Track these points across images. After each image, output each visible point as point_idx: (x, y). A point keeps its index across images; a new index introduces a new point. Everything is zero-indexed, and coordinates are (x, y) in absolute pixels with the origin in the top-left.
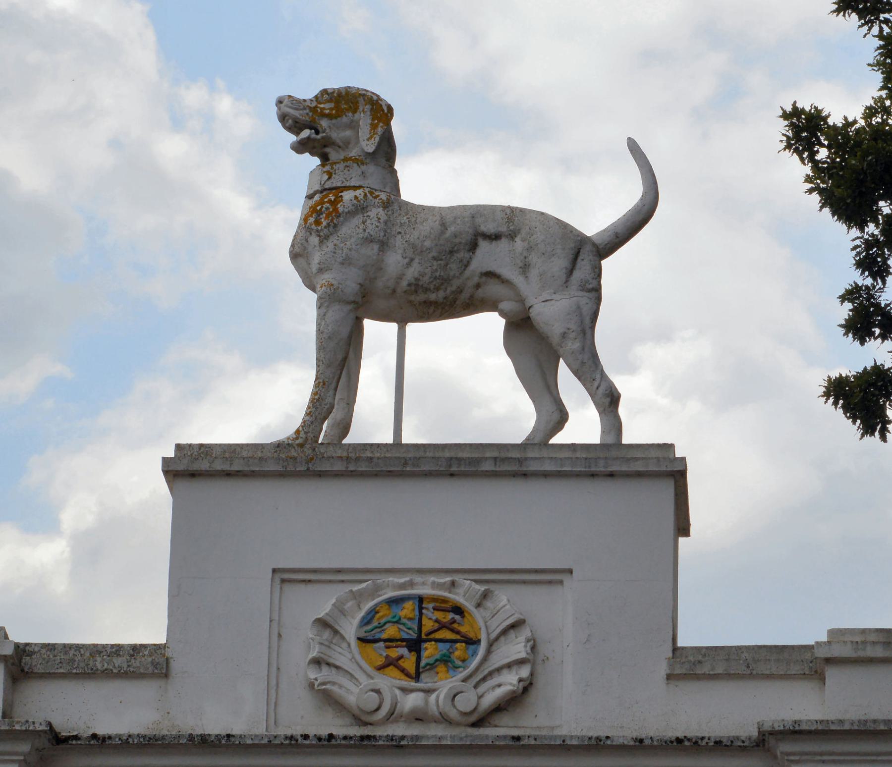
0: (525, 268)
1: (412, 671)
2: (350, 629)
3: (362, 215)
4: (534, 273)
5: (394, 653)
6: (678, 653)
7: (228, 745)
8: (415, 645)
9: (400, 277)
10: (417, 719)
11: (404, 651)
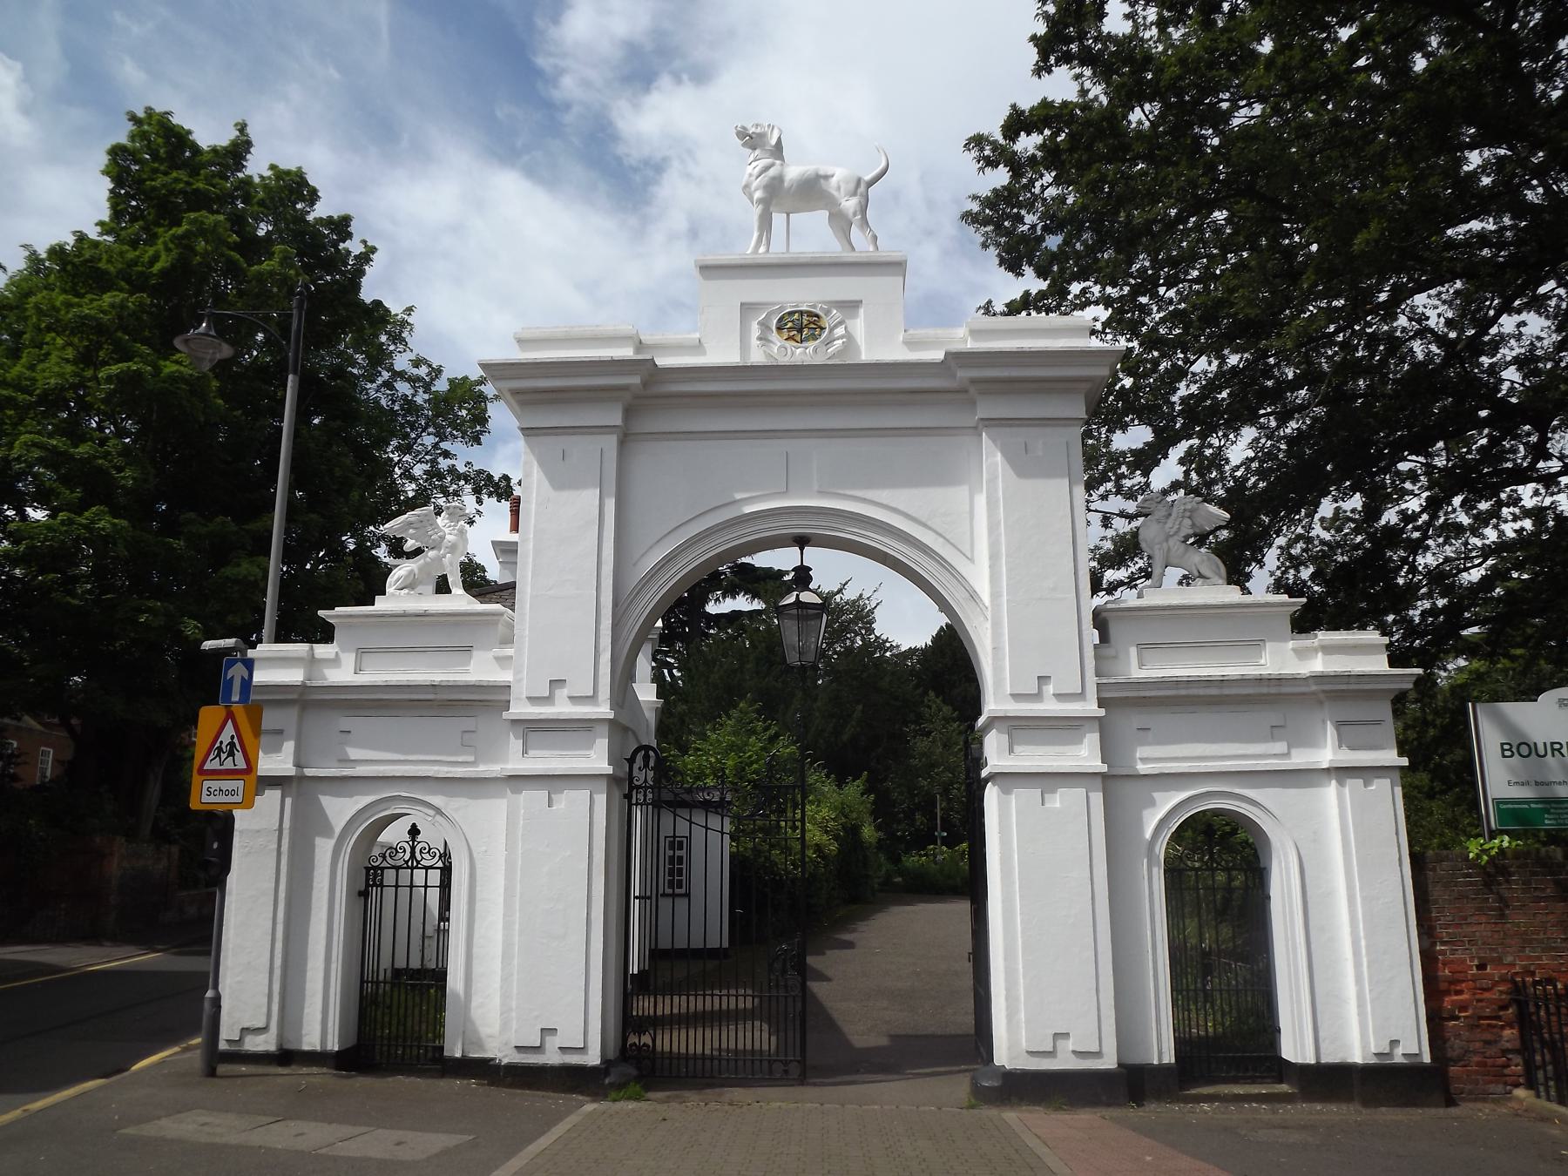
8: (800, 331)
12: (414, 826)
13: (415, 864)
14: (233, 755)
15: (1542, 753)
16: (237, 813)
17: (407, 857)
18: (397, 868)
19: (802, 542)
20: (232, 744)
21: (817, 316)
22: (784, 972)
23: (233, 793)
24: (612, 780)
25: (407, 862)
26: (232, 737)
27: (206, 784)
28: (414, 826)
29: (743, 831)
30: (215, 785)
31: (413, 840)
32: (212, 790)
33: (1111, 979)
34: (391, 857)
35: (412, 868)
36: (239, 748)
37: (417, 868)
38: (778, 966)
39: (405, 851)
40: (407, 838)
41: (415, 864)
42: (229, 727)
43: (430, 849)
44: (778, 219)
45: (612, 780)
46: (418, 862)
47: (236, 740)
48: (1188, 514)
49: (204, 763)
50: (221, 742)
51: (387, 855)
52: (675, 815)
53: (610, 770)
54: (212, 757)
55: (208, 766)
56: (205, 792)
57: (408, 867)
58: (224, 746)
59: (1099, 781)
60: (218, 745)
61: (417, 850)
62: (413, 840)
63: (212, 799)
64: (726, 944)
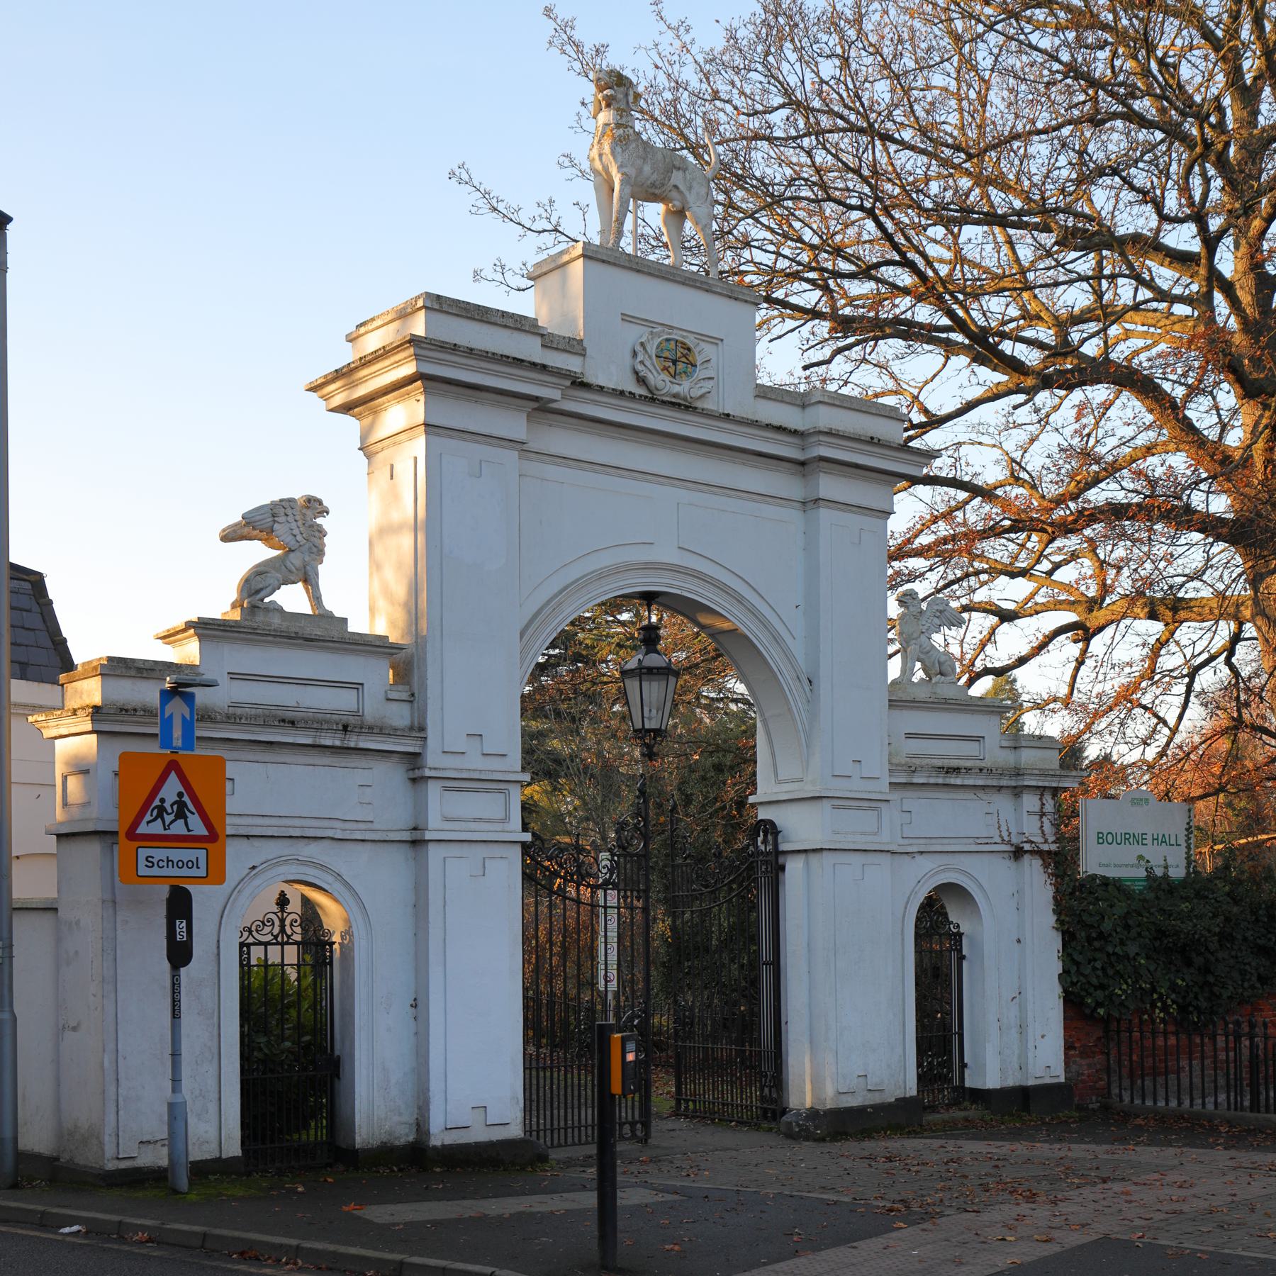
0: (690, 188)
1: (673, 374)
2: (652, 348)
3: (1090, 572)
4: (693, 191)
5: (667, 364)
6: (301, 575)
7: (958, 326)
8: (675, 362)
9: (648, 179)
10: (392, 477)
11: (671, 364)
13: (285, 939)
14: (185, 818)
18: (266, 944)
20: (181, 805)
21: (689, 349)
24: (220, 1157)
26: (180, 795)
27: (143, 853)
28: (283, 894)
30: (159, 854)
31: (282, 911)
32: (155, 861)
33: (431, 896)
34: (257, 931)
35: (282, 944)
36: (193, 810)
37: (288, 943)
39: (273, 924)
40: (275, 908)
41: (285, 939)
43: (263, 922)
45: (220, 1157)
46: (289, 937)
47: (186, 799)
50: (162, 800)
51: (253, 928)
53: (1000, 347)
54: (148, 817)
55: (143, 829)
56: (142, 862)
57: (277, 944)
58: (167, 805)
60: (157, 802)
61: (287, 922)
62: (282, 911)
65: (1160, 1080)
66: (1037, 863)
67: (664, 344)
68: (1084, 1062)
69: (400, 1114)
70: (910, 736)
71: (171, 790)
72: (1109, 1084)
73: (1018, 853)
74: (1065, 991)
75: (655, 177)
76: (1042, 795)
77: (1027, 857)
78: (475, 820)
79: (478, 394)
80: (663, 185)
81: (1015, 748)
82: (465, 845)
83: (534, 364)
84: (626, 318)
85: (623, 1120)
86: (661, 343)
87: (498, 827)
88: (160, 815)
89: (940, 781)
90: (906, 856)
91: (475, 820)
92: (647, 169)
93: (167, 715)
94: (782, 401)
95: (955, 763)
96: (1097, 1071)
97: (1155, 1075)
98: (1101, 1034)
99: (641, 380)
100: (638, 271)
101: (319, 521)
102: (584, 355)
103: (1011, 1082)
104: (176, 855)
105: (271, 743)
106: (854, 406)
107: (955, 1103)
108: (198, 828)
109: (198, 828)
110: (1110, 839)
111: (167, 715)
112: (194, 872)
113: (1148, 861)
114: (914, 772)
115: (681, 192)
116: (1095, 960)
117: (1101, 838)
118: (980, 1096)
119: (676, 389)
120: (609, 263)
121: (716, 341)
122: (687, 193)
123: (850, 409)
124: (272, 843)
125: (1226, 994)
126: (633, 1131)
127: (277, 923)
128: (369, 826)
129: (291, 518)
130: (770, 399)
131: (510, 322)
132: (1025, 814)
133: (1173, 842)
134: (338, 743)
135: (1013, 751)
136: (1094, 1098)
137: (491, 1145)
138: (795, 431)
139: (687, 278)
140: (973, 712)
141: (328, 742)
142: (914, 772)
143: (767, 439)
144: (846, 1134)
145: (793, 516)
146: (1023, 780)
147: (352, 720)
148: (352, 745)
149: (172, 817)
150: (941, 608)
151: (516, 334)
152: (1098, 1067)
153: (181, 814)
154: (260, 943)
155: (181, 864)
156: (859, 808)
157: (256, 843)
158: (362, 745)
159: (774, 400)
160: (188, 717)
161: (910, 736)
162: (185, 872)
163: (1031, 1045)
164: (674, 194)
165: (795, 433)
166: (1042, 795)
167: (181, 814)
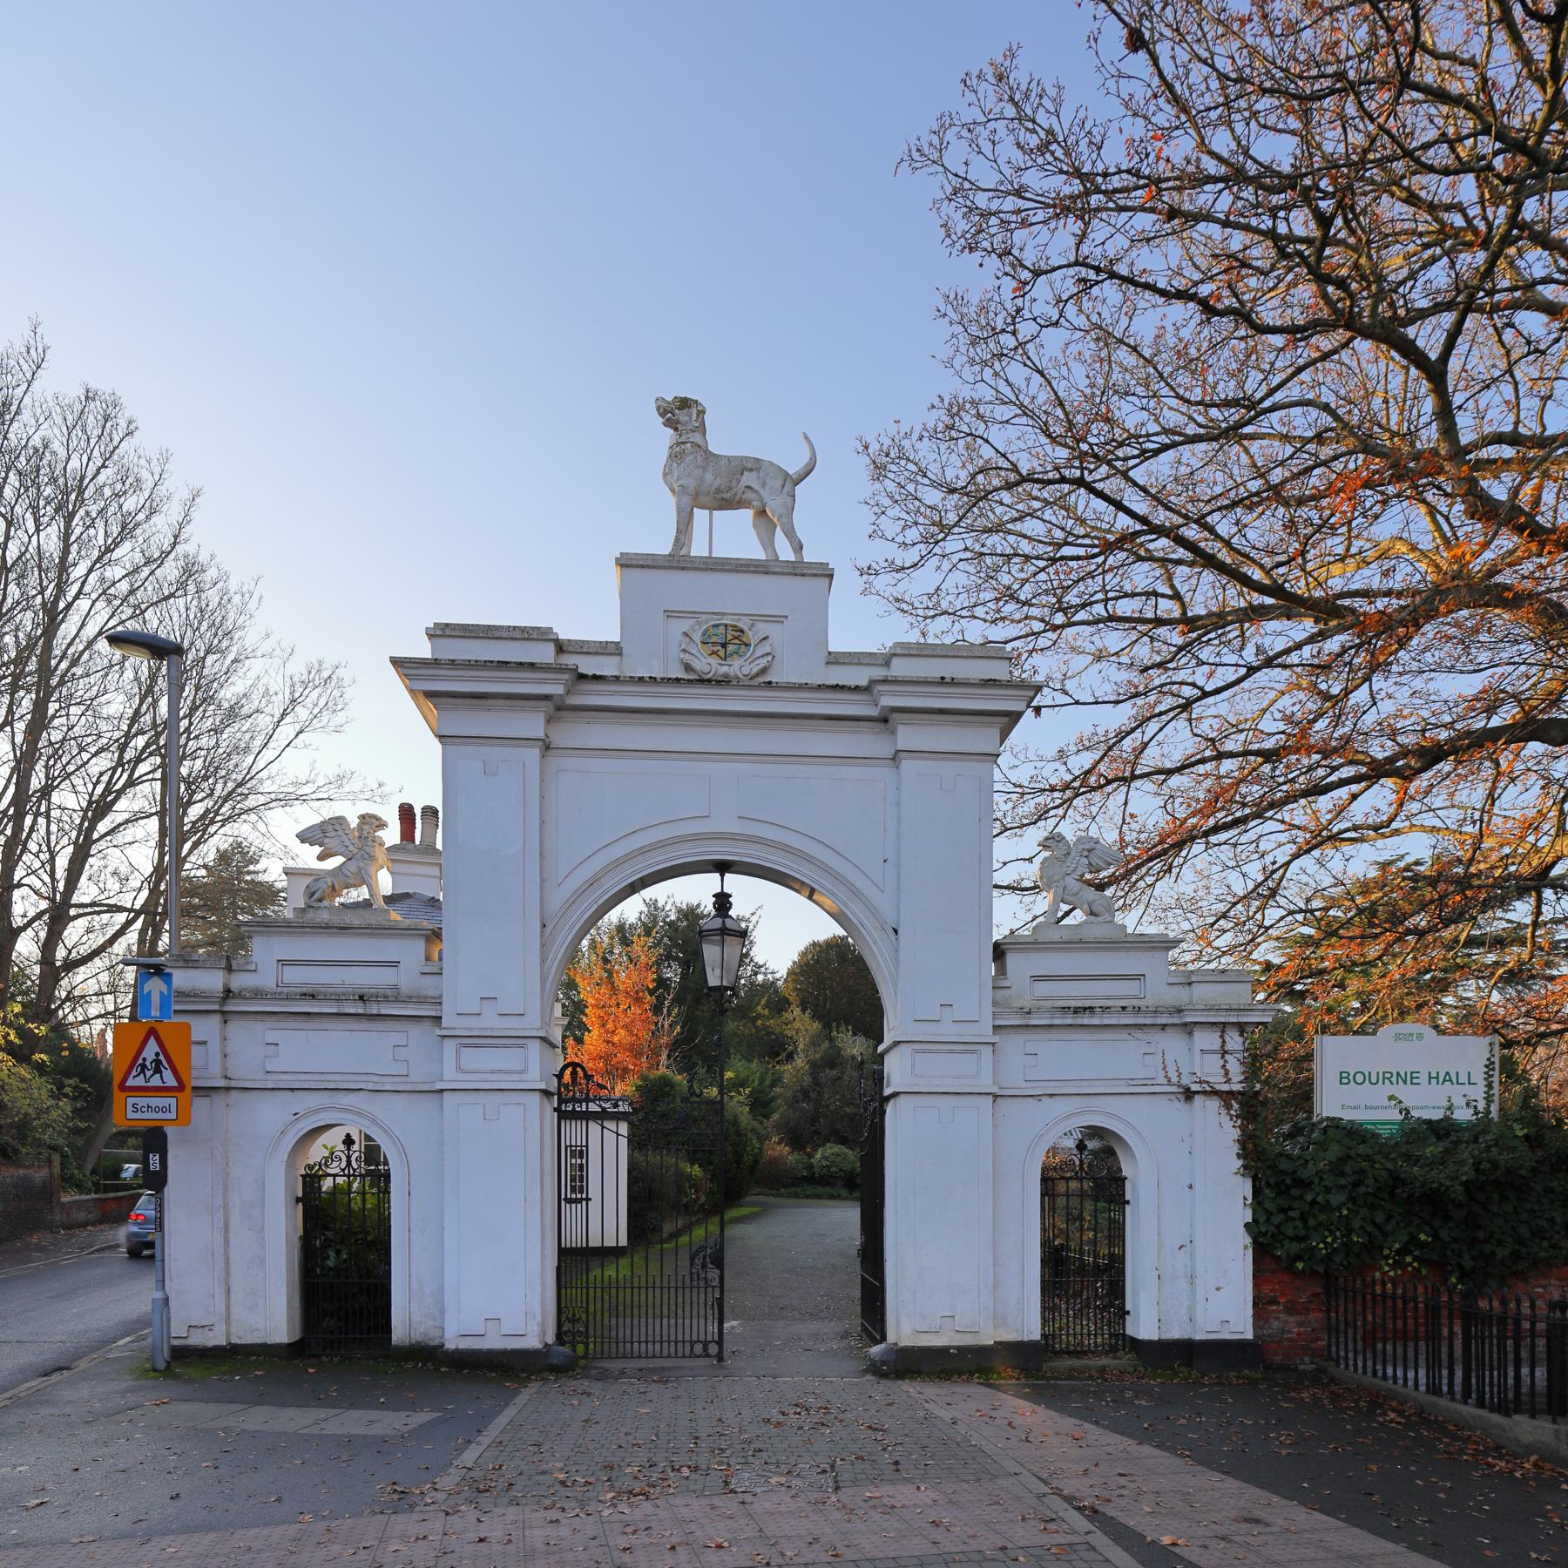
0: (764, 485)
2: (697, 637)
5: (716, 649)
8: (724, 645)
12: (348, 1136)
14: (161, 1072)
15: (1374, 1081)
16: (170, 1131)
17: (343, 1165)
19: (722, 867)
20: (158, 1062)
21: (742, 631)
22: (704, 1266)
23: (166, 1109)
25: (343, 1170)
26: (157, 1054)
27: (131, 1101)
28: (348, 1136)
29: (1462, 967)
30: (142, 1102)
31: (349, 1149)
38: (698, 1261)
40: (342, 1147)
42: (152, 1043)
44: (700, 515)
47: (161, 1057)
48: (1086, 853)
49: (125, 1079)
50: (144, 1059)
52: (603, 1127)
54: (134, 1073)
55: (130, 1082)
58: (148, 1063)
59: (991, 1098)
60: (140, 1061)
61: (353, 1159)
62: (349, 1149)
63: (139, 1115)
64: (623, 1242)
65: (1411, 1345)
66: (1214, 1104)
67: (711, 630)
68: (1291, 1319)
69: (435, 1320)
70: (1037, 978)
71: (151, 1049)
72: (1329, 1346)
73: (1189, 1095)
74: (1255, 1242)
75: (718, 482)
76: (1223, 1032)
77: (1197, 1097)
78: (492, 1072)
79: (491, 702)
80: (731, 488)
81: (1190, 984)
82: (481, 1093)
83: (521, 664)
84: (669, 614)
85: (695, 1338)
86: (707, 630)
87: (515, 1077)
88: (143, 1072)
89: (1069, 1021)
90: (1030, 1099)
91: (492, 1072)
92: (709, 477)
93: (145, 992)
94: (860, 664)
95: (1087, 1004)
96: (1313, 1330)
97: (1405, 1339)
98: (1320, 1290)
99: (688, 668)
100: (683, 569)
101: (379, 833)
102: (621, 654)
103: (1175, 1333)
104: (154, 1102)
105: (309, 1014)
106: (938, 652)
107: (1113, 1350)
108: (171, 1081)
109: (171, 1081)
110: (1359, 1078)
111: (145, 992)
112: (167, 1116)
113: (1400, 1102)
114: (1029, 1013)
115: (755, 491)
116: (1291, 1208)
117: (1344, 1079)
118: (1136, 1345)
119: (725, 669)
120: (648, 567)
121: (779, 619)
122: (762, 492)
123: (933, 656)
124: (314, 1094)
125: (1502, 1253)
126: (705, 1349)
127: (344, 1159)
128: (404, 1079)
129: (340, 833)
130: (844, 663)
131: (517, 634)
132: (1197, 1054)
133: (1463, 1079)
134: (361, 1011)
135: (1187, 987)
136: (1307, 1359)
137: (504, 1353)
138: (857, 687)
139: (737, 565)
140: (1128, 949)
141: (352, 1011)
142: (1029, 1013)
143: (829, 701)
144: (919, 1373)
145: (885, 773)
146: (1185, 1016)
147: (389, 992)
148: (375, 1012)
149: (151, 1072)
150: (1087, 846)
151: (527, 644)
152: (1315, 1325)
153: (158, 1070)
154: (1062, 1178)
155: (158, 1109)
156: (951, 1052)
157: (300, 1094)
158: (384, 1012)
159: (850, 664)
160: (166, 993)
161: (1037, 978)
162: (161, 1116)
163: (1200, 1297)
164: (749, 495)
165: (857, 689)
166: (1223, 1032)
167: (158, 1070)
